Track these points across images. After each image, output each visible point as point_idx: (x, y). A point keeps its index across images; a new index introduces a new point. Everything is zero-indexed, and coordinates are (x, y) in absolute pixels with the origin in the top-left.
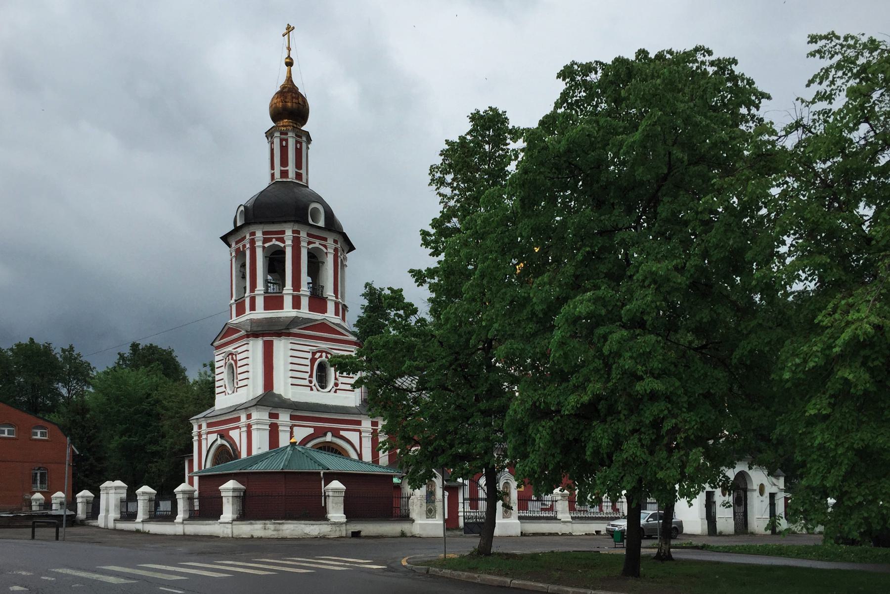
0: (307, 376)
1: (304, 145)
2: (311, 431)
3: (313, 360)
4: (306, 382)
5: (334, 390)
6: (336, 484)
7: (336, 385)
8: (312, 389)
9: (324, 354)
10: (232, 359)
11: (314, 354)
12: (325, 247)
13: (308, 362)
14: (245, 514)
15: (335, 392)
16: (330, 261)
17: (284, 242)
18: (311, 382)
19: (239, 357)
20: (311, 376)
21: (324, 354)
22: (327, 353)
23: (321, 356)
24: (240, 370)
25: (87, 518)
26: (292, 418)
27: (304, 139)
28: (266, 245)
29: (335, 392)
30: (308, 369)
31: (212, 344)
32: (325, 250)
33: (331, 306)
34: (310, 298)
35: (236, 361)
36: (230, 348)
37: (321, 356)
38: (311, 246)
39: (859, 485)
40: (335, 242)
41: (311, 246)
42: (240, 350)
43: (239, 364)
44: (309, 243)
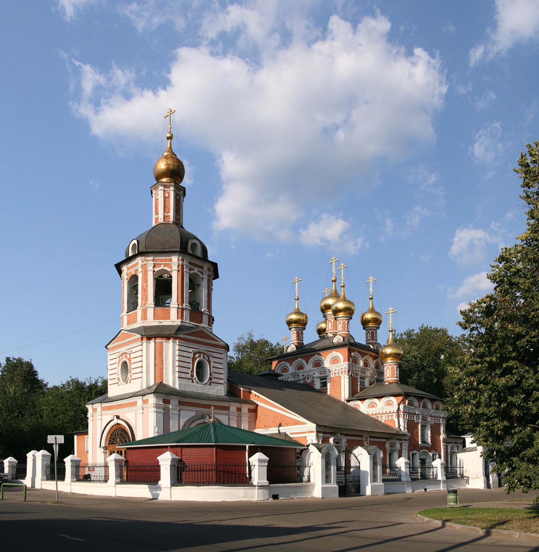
0: (190, 371)
1: (182, 197)
2: (193, 414)
3: (194, 359)
4: (189, 376)
5: (209, 382)
6: (259, 456)
7: (210, 379)
8: (193, 382)
9: (202, 355)
10: (126, 357)
11: (195, 354)
12: (202, 273)
13: (190, 360)
14: (180, 477)
15: (210, 384)
16: (204, 283)
17: (171, 268)
18: (192, 376)
19: (133, 356)
20: (192, 371)
21: (202, 355)
22: (204, 354)
23: (200, 356)
24: (133, 366)
25: (12, 479)
26: (181, 403)
27: (182, 192)
28: (156, 270)
29: (210, 384)
30: (190, 366)
31: (106, 347)
32: (202, 276)
33: (205, 318)
34: (191, 311)
35: (130, 360)
36: (123, 349)
37: (200, 356)
38: (191, 272)
39: (294, 476)
40: (209, 270)
41: (191, 272)
42: (134, 350)
43: (133, 361)
44: (190, 270)
